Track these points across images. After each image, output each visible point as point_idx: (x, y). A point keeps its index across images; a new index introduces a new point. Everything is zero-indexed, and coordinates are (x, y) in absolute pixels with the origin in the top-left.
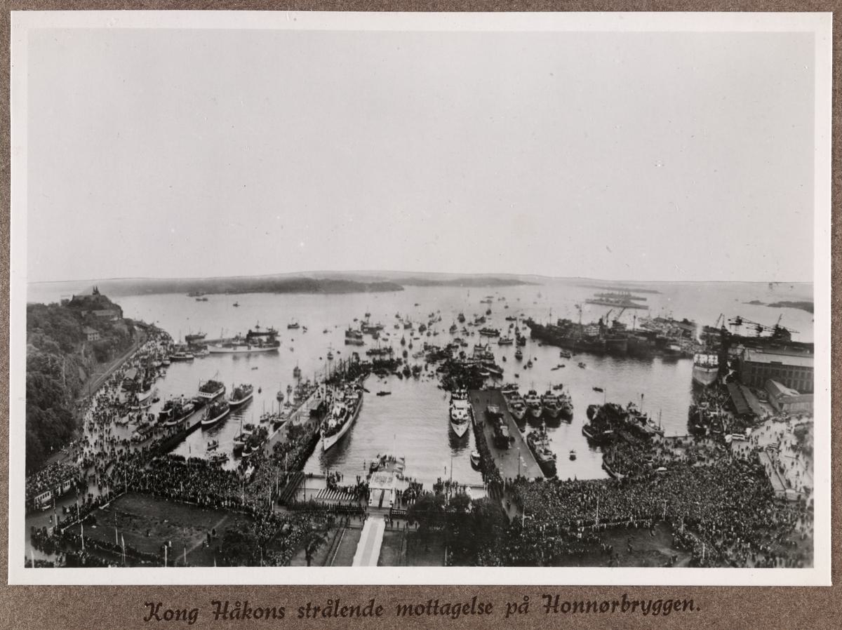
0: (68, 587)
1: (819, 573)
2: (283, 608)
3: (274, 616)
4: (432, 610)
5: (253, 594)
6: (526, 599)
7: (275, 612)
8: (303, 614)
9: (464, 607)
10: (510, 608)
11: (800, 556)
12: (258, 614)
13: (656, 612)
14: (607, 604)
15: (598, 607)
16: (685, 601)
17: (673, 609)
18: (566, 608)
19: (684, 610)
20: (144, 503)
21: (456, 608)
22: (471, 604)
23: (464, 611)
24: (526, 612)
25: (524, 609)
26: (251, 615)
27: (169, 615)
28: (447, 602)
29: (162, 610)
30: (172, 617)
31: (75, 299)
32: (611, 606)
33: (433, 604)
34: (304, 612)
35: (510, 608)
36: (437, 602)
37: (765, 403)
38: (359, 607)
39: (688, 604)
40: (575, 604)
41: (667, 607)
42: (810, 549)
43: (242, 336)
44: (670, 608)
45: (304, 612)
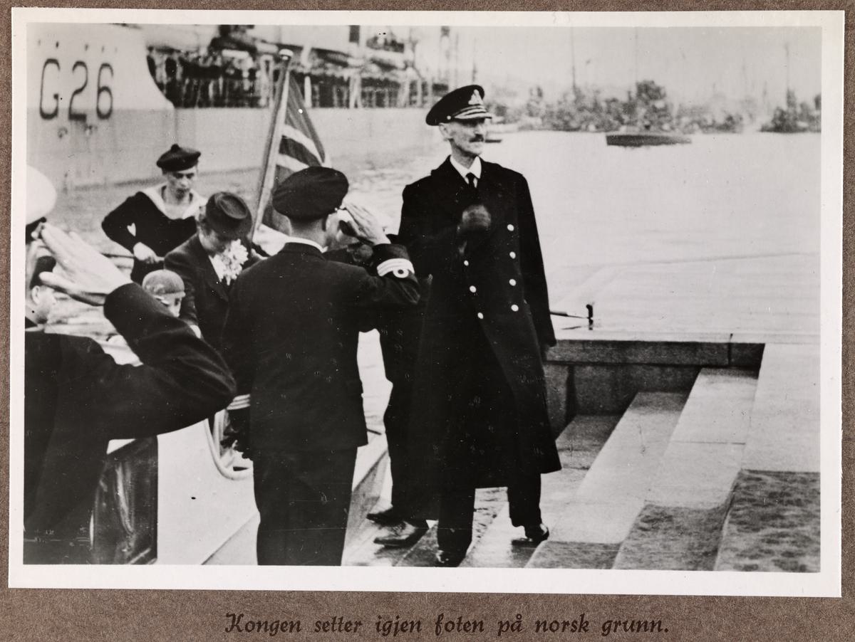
0: (94, 593)
1: (824, 580)
4: (336, 626)
6: (519, 617)
7: (545, 625)
9: (282, 624)
10: (502, 626)
11: (34, 555)
13: (274, 632)
15: (547, 626)
16: (653, 622)
17: (279, 629)
21: (274, 626)
23: (324, 628)
24: (519, 631)
25: (515, 626)
27: (450, 626)
29: (244, 620)
30: (453, 628)
31: (319, 224)
33: (337, 621)
35: (502, 626)
36: (341, 619)
38: (266, 623)
39: (656, 625)
41: (606, 628)
43: (217, 257)
45: (385, 628)
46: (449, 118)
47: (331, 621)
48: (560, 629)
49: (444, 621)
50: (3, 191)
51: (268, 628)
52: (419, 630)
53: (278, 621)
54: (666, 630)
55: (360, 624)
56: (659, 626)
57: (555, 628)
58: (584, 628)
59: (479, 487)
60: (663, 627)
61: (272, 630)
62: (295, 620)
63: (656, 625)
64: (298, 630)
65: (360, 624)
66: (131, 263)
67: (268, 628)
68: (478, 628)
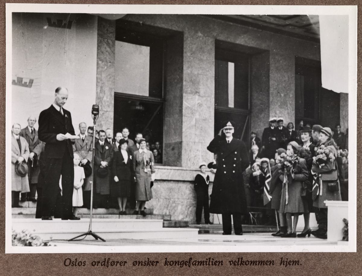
2: (85, 262)
3: (142, 265)
5: (196, 255)
8: (84, 263)
12: (247, 263)
14: (114, 262)
17: (184, 264)
18: (80, 264)
19: (293, 265)
20: (97, 182)
21: (182, 263)
22: (237, 261)
26: (244, 264)
28: (195, 260)
32: (116, 264)
34: (93, 264)
37: (338, 175)
39: (296, 262)
40: (175, 261)
42: (233, 237)
44: (183, 264)
46: (216, 105)
47: (237, 260)
48: (138, 264)
49: (110, 261)
50: (2, 64)
51: (180, 264)
52: (222, 265)
53: (184, 261)
54: (301, 265)
55: (126, 263)
56: (298, 263)
57: (112, 263)
58: (242, 264)
59: (352, 254)
60: (299, 264)
61: (181, 265)
62: (297, 260)
63: (296, 262)
64: (273, 264)
65: (126, 263)
66: (123, 132)
67: (180, 264)
68: (220, 264)
